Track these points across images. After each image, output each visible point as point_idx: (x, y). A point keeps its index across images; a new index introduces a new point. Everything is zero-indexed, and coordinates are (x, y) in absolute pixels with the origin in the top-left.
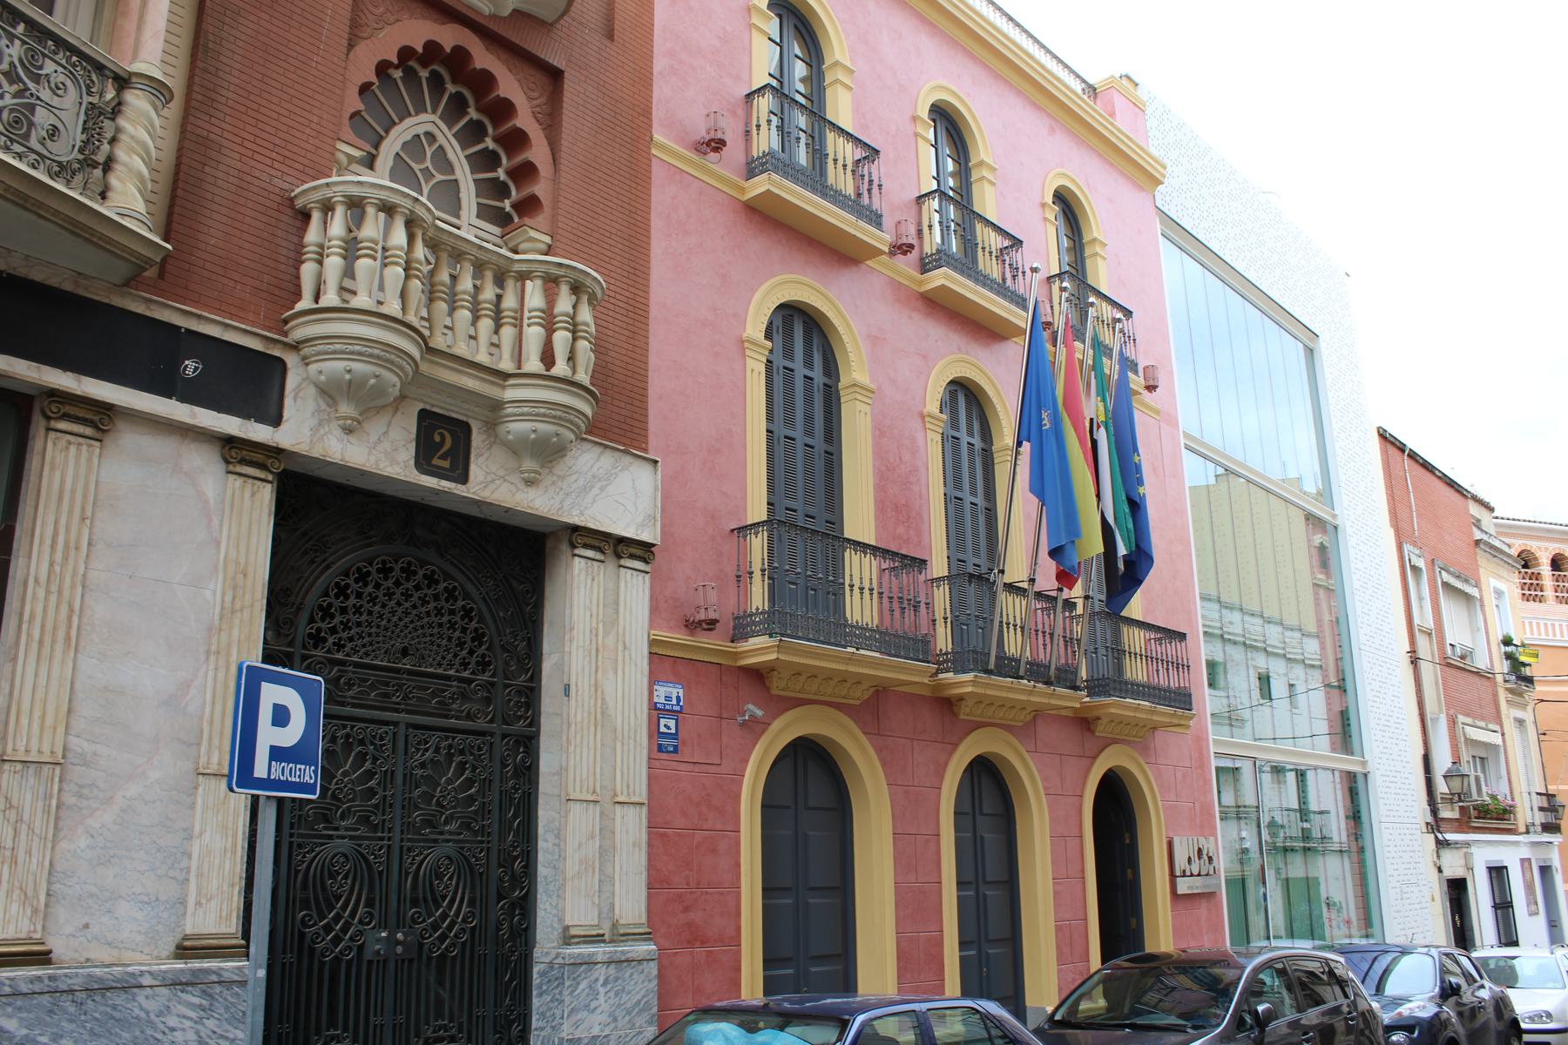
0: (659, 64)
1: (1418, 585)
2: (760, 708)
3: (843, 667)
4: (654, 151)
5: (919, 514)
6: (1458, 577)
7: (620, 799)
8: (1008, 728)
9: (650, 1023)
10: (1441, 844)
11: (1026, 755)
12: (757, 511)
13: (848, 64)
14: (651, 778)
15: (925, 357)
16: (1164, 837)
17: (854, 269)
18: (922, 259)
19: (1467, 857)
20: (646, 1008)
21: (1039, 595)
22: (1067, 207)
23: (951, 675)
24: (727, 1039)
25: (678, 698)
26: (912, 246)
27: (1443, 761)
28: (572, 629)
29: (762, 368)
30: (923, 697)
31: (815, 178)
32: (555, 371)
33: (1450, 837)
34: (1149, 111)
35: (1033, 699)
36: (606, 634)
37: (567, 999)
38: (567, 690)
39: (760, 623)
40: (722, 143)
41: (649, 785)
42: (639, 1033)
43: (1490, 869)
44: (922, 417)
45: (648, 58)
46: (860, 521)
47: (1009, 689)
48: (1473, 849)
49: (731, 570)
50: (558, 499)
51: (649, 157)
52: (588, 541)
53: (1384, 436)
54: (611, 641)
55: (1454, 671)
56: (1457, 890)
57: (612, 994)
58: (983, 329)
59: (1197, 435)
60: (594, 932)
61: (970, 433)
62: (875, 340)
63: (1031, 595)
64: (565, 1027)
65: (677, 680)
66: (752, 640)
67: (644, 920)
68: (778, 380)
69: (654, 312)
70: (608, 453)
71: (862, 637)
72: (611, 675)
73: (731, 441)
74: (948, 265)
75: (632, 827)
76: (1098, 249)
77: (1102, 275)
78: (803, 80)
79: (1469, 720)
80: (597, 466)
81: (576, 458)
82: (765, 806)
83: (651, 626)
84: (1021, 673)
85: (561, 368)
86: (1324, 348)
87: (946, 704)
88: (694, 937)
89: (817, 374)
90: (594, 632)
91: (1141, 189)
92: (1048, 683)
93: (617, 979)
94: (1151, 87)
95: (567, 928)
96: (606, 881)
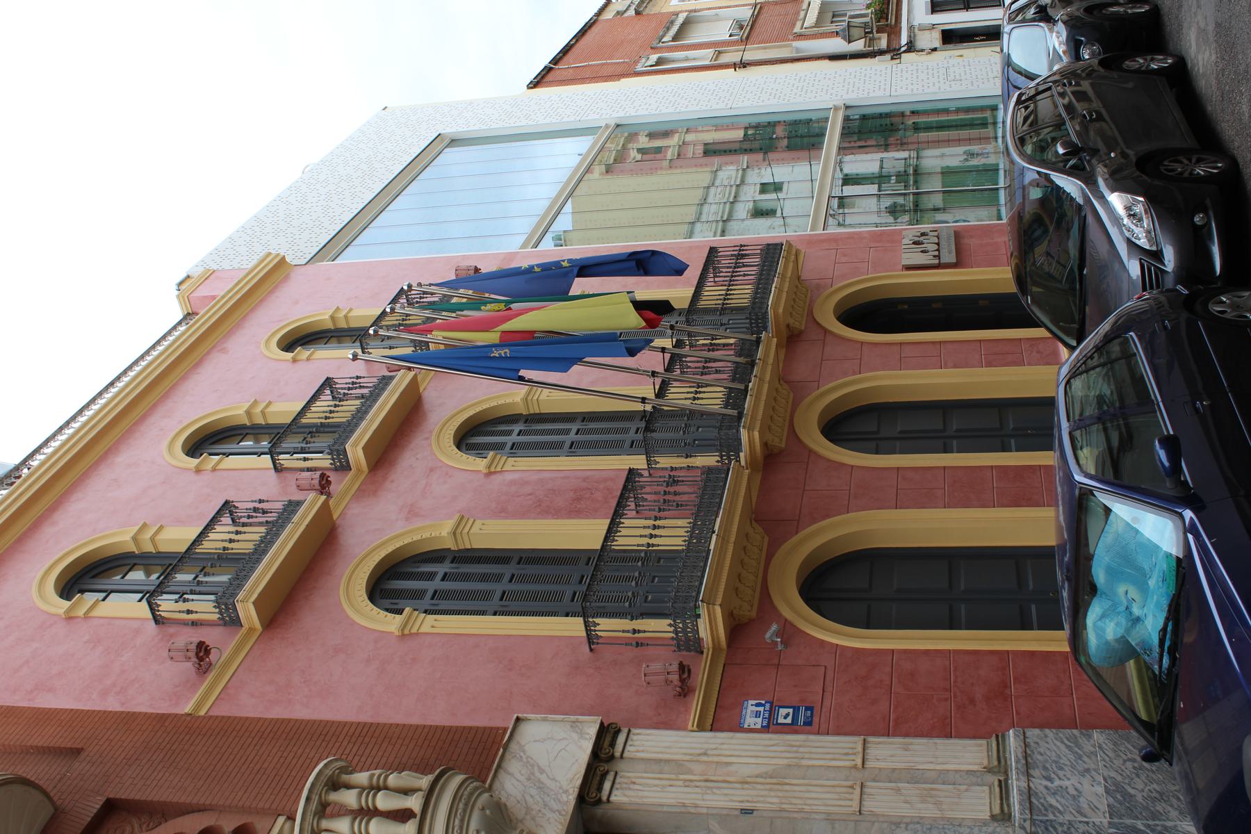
0: (113, 704)
1: (673, 61)
2: (769, 628)
3: (731, 548)
4: (202, 713)
5: (585, 479)
6: (668, 29)
7: (859, 762)
8: (795, 405)
9: (1089, 737)
10: (911, 47)
11: (822, 390)
12: (573, 627)
13: (136, 528)
14: (838, 733)
15: (432, 470)
16: (903, 270)
17: (340, 530)
18: (336, 469)
19: (922, 28)
20: (1075, 740)
21: (669, 369)
22: (300, 340)
23: (742, 455)
24: (1103, 617)
25: (758, 705)
26: (322, 476)
27: (837, 45)
28: (684, 805)
29: (431, 618)
30: (764, 479)
31: (243, 564)
32: (417, 808)
33: (904, 40)
34: (215, 267)
35: (768, 377)
36: (690, 772)
37: (1068, 817)
38: (746, 812)
39: (684, 622)
40: (201, 645)
41: (846, 734)
42: (1100, 747)
43: (933, 11)
44: (489, 474)
45: (105, 715)
46: (585, 534)
47: (757, 398)
48: (916, 23)
49: (631, 653)
50: (549, 815)
51: (208, 718)
52: (595, 785)
53: (536, 83)
54: (697, 768)
55: (754, 34)
56: (951, 37)
57: (1061, 773)
58: (410, 414)
59: (524, 237)
60: (997, 790)
61: (509, 433)
62: (412, 512)
63: (668, 376)
64: (1097, 821)
65: (740, 706)
66: (702, 634)
67: (984, 742)
68: (444, 605)
69: (365, 718)
70: (504, 765)
71: (699, 534)
72: (732, 768)
73: (502, 648)
74: (343, 444)
75: (888, 752)
76: (341, 315)
77: (364, 312)
78: (148, 574)
79: (799, 24)
80: (518, 775)
81: (509, 795)
82: (868, 626)
83: (685, 729)
84: (742, 387)
85: (414, 803)
86: (451, 128)
87: (770, 460)
88: (1000, 694)
89: (441, 569)
90: (688, 783)
91: (287, 278)
92: (753, 364)
93: (1045, 768)
94: (188, 261)
95: (993, 817)
96: (943, 777)
